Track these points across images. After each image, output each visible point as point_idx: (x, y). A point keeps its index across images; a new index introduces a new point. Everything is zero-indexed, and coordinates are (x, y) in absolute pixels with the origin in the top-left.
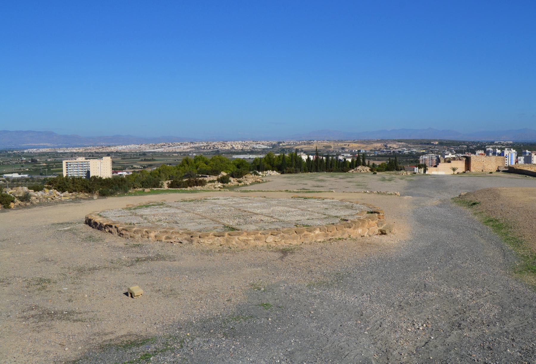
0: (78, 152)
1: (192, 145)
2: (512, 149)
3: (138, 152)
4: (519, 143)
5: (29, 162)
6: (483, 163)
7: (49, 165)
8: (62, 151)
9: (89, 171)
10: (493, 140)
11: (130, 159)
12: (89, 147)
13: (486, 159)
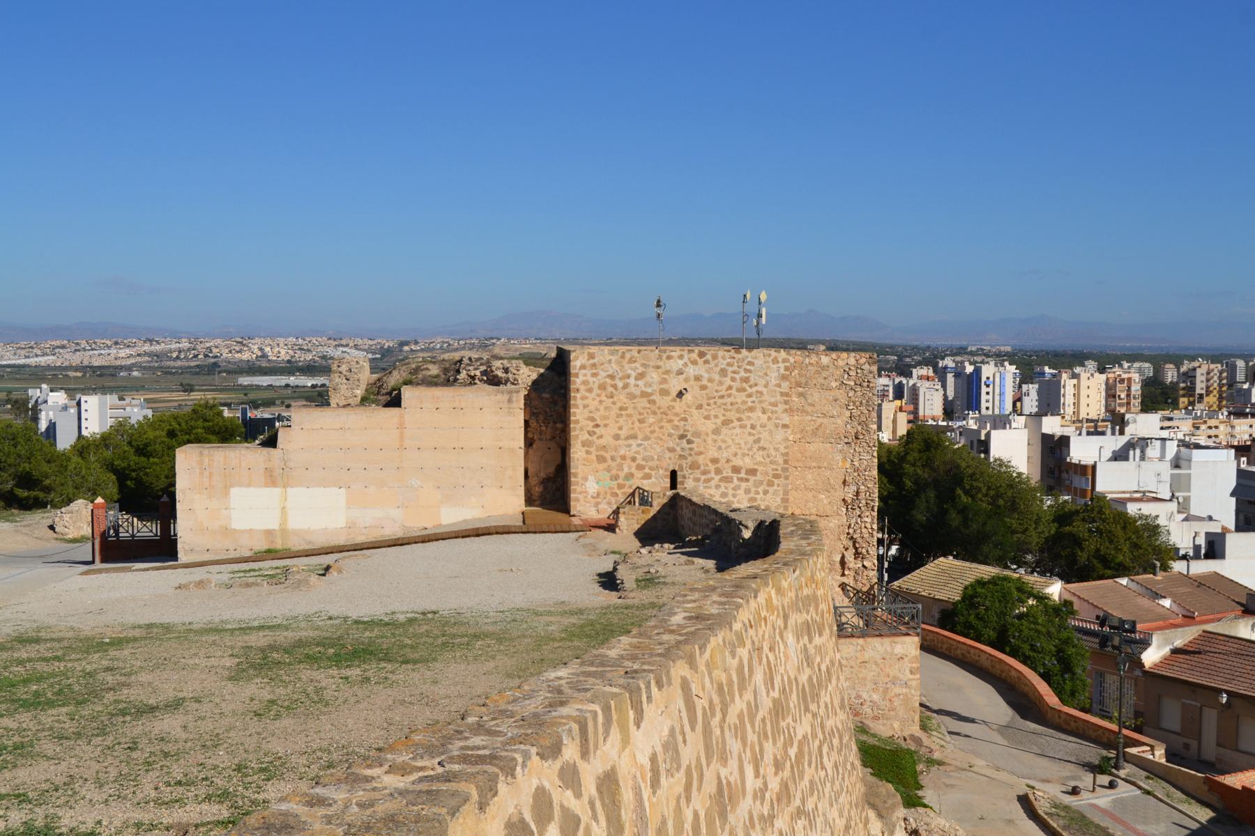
2: (1006, 364)
4: (1027, 351)
6: (679, 406)
10: (964, 343)
13: (700, 370)
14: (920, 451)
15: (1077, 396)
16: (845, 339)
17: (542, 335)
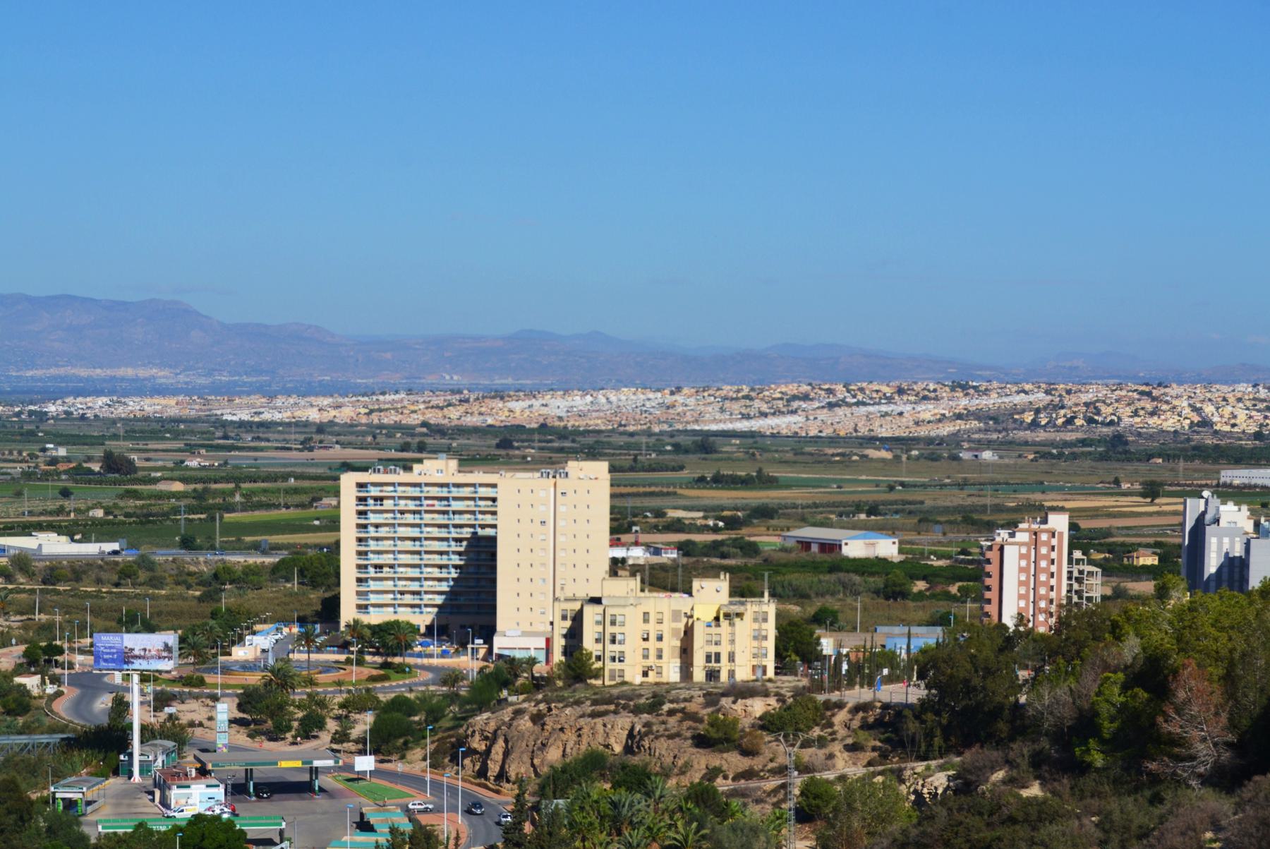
0: (332, 423)
1: (963, 403)
3: (662, 433)
5: (90, 471)
7: (205, 490)
8: (244, 416)
9: (492, 540)
11: (632, 469)
12: (388, 398)
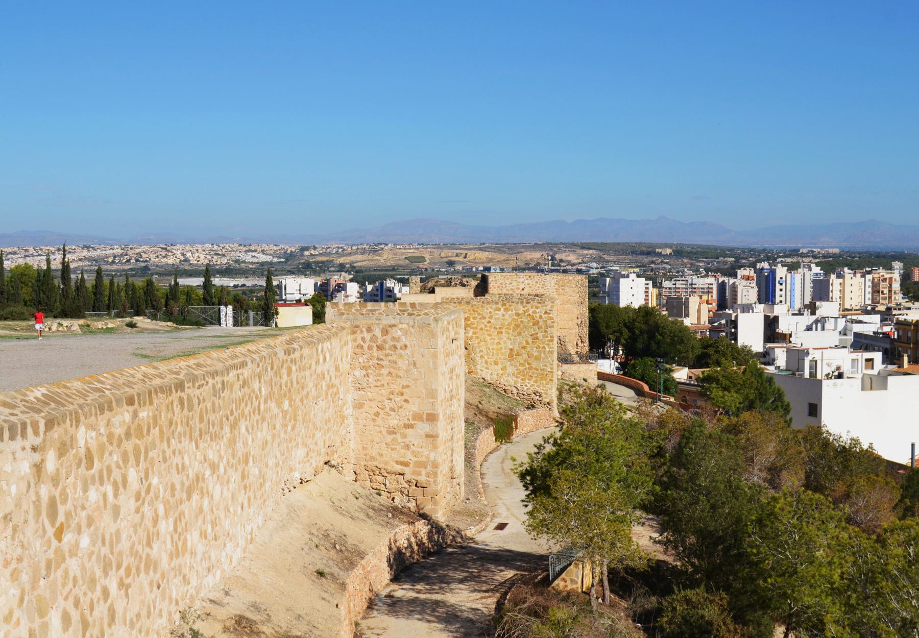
13: (529, 281)
14: (643, 317)
15: (842, 291)
16: (690, 243)
17: (423, 240)
